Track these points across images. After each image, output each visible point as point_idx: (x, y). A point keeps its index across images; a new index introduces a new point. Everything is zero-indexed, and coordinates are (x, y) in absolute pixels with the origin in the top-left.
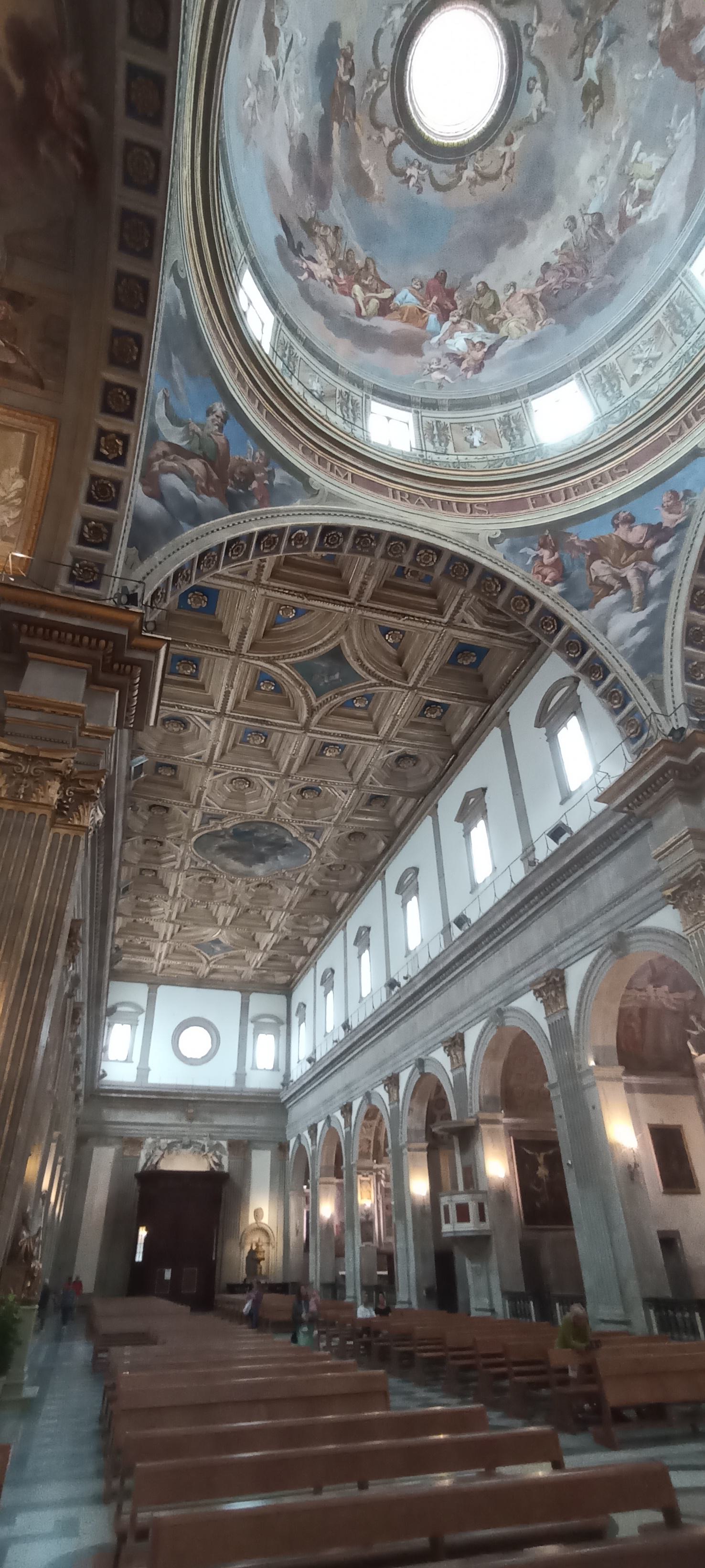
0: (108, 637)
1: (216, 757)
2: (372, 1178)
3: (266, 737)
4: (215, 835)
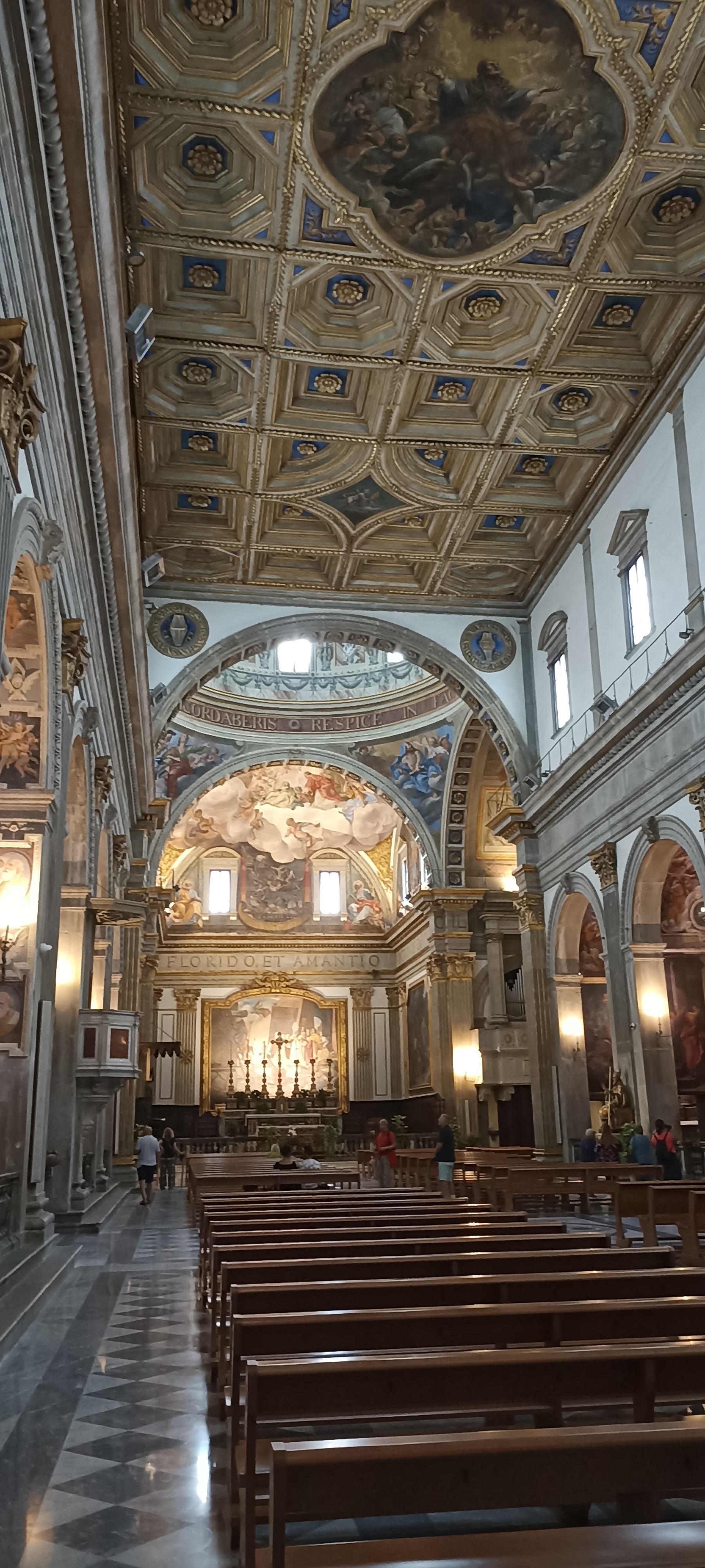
3: (344, 380)
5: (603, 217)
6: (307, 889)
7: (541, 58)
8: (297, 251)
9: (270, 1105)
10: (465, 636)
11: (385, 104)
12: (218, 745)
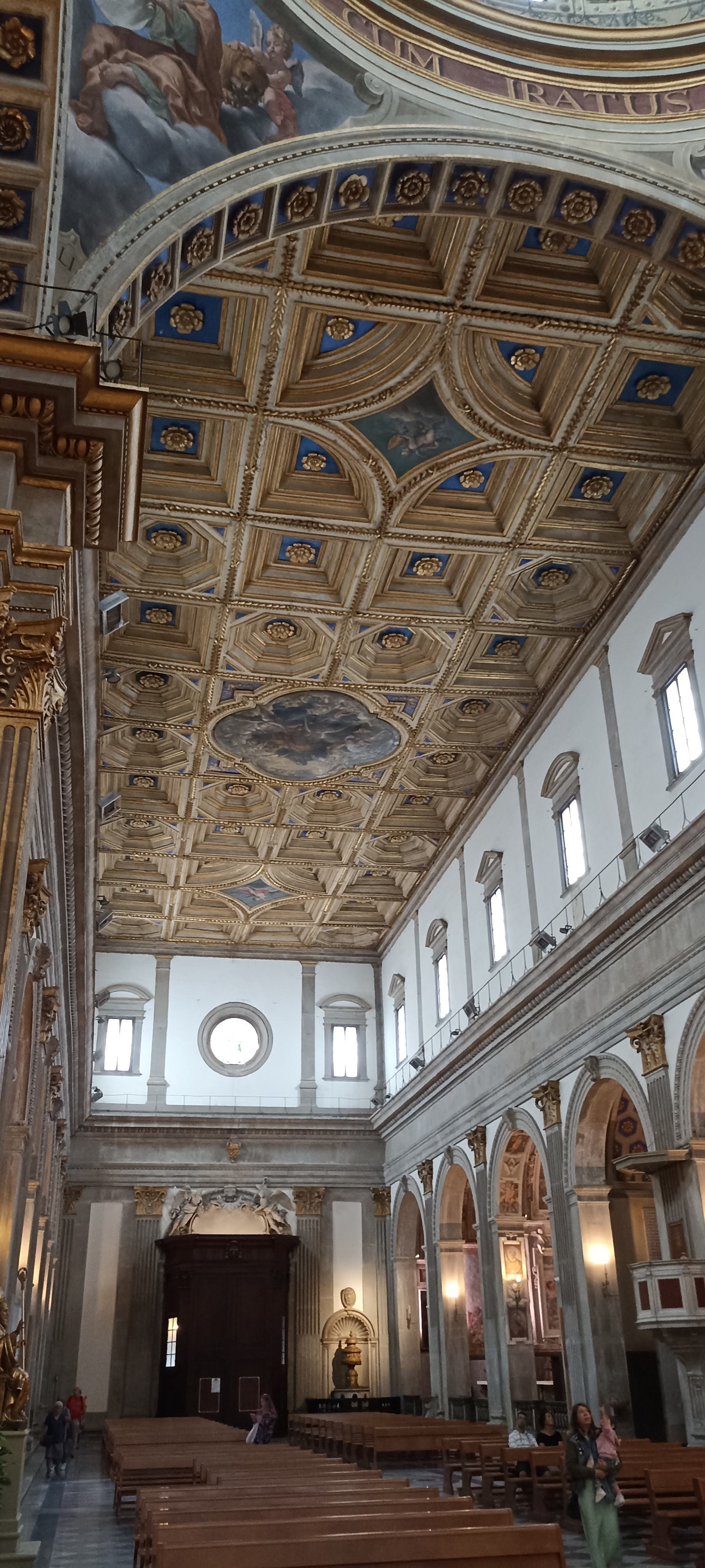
0: (45, 393)
1: (237, 588)
2: (524, 1241)
3: (317, 550)
4: (244, 716)
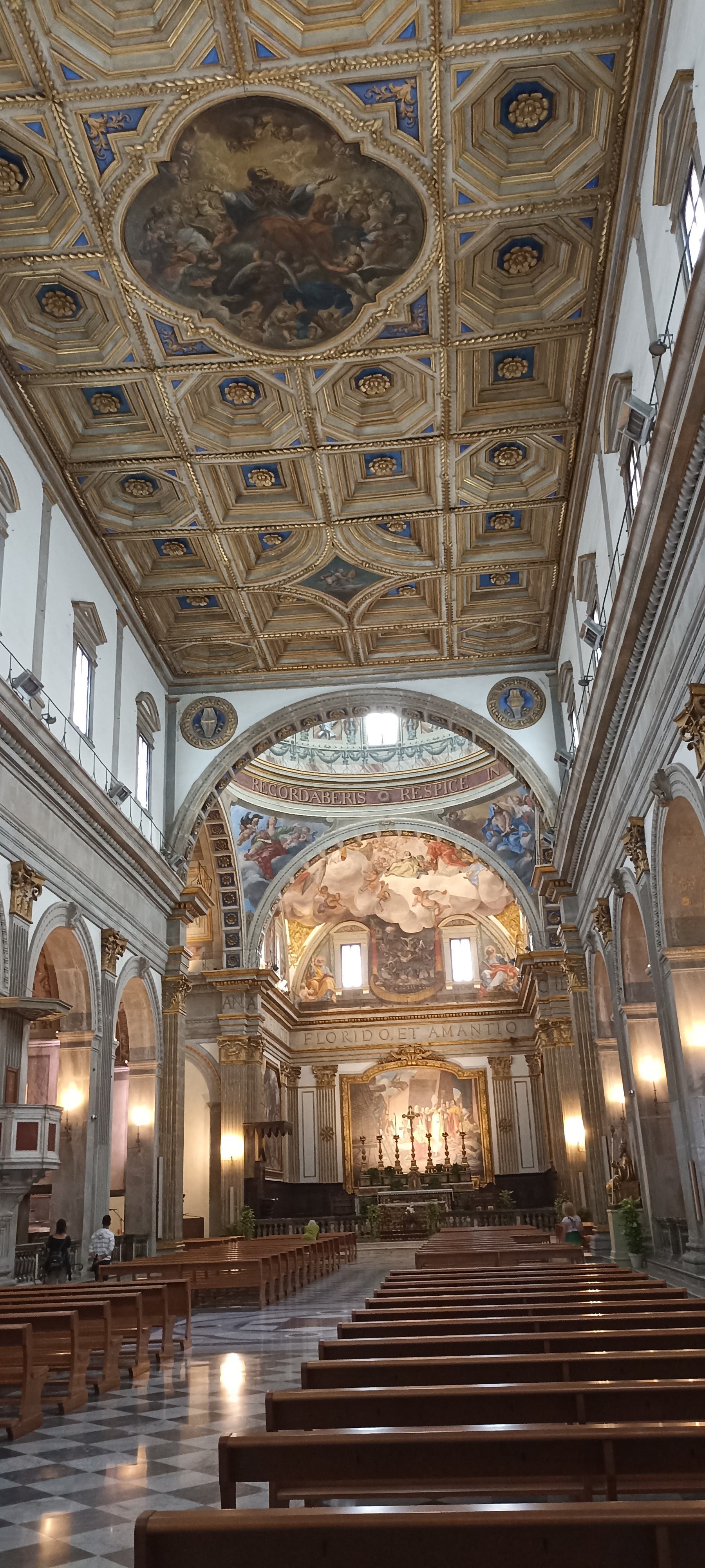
5: (439, 284)
6: (438, 958)
7: (303, 155)
8: (167, 367)
9: (403, 1181)
10: (492, 695)
11: (181, 225)
12: (309, 824)
